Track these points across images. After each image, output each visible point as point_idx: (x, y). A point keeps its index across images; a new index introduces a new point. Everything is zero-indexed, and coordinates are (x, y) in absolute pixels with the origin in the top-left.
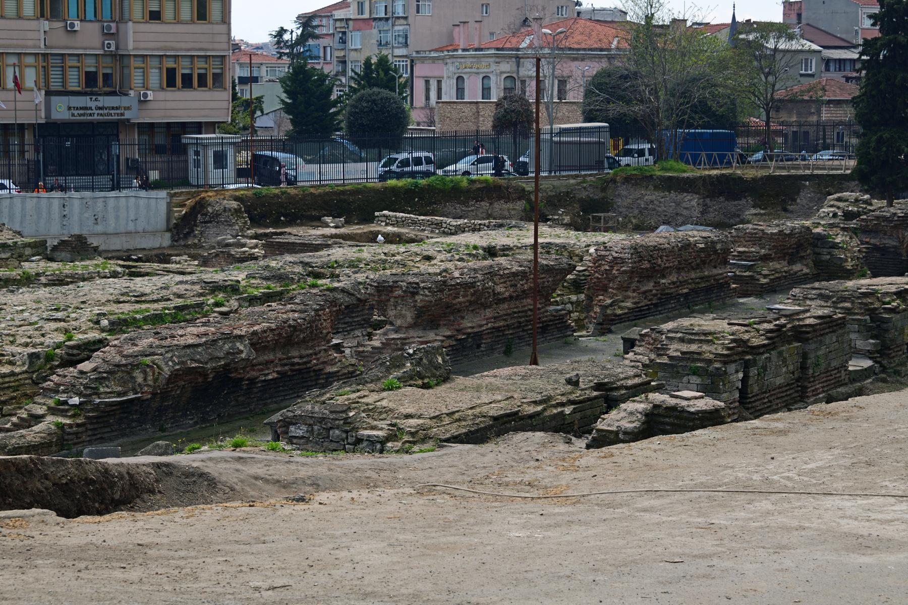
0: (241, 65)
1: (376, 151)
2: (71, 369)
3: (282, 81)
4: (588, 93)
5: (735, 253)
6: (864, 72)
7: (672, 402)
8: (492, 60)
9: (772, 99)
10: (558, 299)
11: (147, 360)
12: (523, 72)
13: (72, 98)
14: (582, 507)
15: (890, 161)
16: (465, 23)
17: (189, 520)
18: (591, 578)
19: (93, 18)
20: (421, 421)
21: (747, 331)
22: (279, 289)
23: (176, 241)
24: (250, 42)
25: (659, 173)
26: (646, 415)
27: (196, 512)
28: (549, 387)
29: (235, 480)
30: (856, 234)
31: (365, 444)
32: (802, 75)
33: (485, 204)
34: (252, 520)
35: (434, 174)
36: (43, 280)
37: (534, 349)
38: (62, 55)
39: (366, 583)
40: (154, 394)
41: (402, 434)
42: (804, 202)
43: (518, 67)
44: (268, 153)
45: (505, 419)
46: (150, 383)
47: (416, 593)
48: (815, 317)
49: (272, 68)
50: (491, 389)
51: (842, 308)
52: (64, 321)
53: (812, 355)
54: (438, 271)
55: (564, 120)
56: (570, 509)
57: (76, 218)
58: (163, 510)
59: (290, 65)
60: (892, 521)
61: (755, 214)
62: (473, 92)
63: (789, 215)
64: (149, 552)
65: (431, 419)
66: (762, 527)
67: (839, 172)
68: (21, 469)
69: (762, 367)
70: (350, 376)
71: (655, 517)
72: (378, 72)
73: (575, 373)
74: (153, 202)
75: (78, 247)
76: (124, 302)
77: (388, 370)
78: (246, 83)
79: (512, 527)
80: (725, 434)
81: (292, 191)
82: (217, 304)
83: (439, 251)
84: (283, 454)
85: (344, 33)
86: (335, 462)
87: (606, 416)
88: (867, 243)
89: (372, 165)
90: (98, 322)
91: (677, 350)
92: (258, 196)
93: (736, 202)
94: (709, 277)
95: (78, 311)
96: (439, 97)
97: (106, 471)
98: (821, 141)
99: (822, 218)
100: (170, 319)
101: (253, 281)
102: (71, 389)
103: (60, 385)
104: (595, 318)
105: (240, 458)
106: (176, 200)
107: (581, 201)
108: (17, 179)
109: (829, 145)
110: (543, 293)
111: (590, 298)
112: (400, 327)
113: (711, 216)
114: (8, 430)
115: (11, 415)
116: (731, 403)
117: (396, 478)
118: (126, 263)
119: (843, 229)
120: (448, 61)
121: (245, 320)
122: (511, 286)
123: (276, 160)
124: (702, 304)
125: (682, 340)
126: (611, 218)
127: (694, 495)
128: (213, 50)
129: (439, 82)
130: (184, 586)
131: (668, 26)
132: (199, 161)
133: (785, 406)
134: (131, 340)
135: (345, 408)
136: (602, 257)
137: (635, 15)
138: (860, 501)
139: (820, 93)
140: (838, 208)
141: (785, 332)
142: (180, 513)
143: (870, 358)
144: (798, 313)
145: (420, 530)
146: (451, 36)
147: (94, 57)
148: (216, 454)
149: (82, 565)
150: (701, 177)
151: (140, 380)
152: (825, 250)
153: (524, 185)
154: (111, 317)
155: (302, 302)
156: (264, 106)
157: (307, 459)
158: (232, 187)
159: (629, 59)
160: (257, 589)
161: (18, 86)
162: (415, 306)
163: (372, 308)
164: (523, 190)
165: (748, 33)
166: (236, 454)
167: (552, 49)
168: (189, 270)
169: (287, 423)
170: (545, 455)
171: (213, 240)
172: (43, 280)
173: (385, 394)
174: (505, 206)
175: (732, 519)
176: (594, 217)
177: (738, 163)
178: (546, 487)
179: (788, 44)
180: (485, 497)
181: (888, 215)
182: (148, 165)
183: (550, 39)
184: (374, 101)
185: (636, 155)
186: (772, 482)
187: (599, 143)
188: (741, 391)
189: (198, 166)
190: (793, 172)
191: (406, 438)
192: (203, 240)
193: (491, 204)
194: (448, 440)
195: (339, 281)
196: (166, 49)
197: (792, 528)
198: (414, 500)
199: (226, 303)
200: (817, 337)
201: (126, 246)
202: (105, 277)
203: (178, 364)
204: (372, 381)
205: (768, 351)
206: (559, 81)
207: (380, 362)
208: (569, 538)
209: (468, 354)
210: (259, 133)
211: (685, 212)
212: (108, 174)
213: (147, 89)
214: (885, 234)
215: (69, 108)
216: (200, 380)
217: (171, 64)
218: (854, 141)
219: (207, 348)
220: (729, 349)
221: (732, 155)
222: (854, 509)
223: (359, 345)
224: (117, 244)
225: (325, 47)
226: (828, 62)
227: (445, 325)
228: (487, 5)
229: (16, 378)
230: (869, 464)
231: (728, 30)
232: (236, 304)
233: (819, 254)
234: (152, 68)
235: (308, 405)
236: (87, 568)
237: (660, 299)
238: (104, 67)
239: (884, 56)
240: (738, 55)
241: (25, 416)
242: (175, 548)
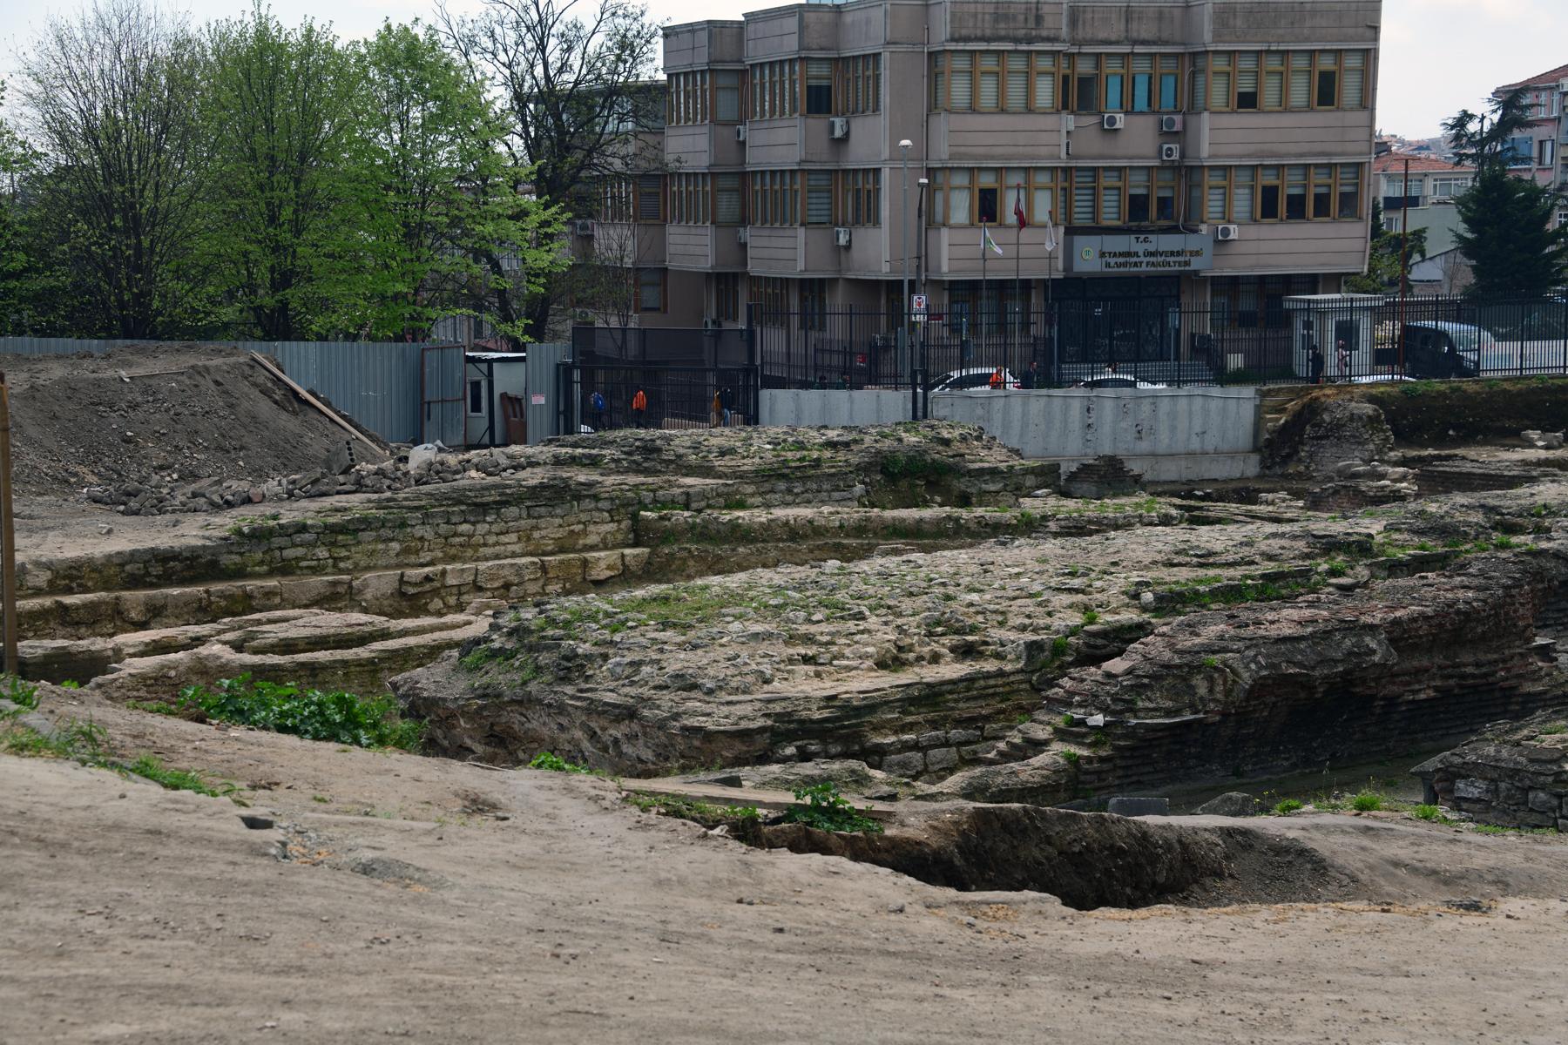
0: (1390, 178)
2: (1093, 669)
3: (1460, 202)
11: (1216, 659)
17: (1278, 927)
19: (1145, 109)
22: (1440, 550)
24: (1408, 138)
27: (1291, 914)
29: (1360, 865)
38: (1094, 169)
40: (1225, 715)
44: (1431, 324)
46: (1219, 696)
49: (1444, 180)
52: (1083, 592)
58: (1235, 907)
64: (1212, 975)
68: (1008, 824)
74: (1232, 405)
75: (1109, 475)
81: (1469, 386)
82: (1333, 573)
84: (1444, 827)
92: (1409, 394)
100: (1254, 594)
101: (1396, 536)
102: (1092, 701)
105: (1368, 829)
114: (991, 762)
115: (997, 738)
121: (1381, 599)
123: (1444, 335)
128: (1342, 154)
132: (1310, 337)
135: (1557, 755)
142: (1262, 914)
148: (1327, 819)
149: (1101, 988)
151: (1202, 690)
154: (1159, 589)
156: (1427, 245)
157: (1486, 839)
158: (1365, 380)
166: (1362, 822)
168: (1289, 515)
169: (1451, 775)
171: (1331, 467)
172: (1053, 526)
192: (1313, 466)
195: (1549, 539)
202: (1151, 524)
203: (1265, 668)
210: (1416, 291)
213: (1230, 222)
215: (1102, 255)
216: (1302, 695)
217: (1269, 180)
224: (1170, 471)
225: (1541, 143)
232: (1366, 573)
235: (1490, 746)
236: (1108, 994)
241: (1017, 741)
242: (1254, 971)
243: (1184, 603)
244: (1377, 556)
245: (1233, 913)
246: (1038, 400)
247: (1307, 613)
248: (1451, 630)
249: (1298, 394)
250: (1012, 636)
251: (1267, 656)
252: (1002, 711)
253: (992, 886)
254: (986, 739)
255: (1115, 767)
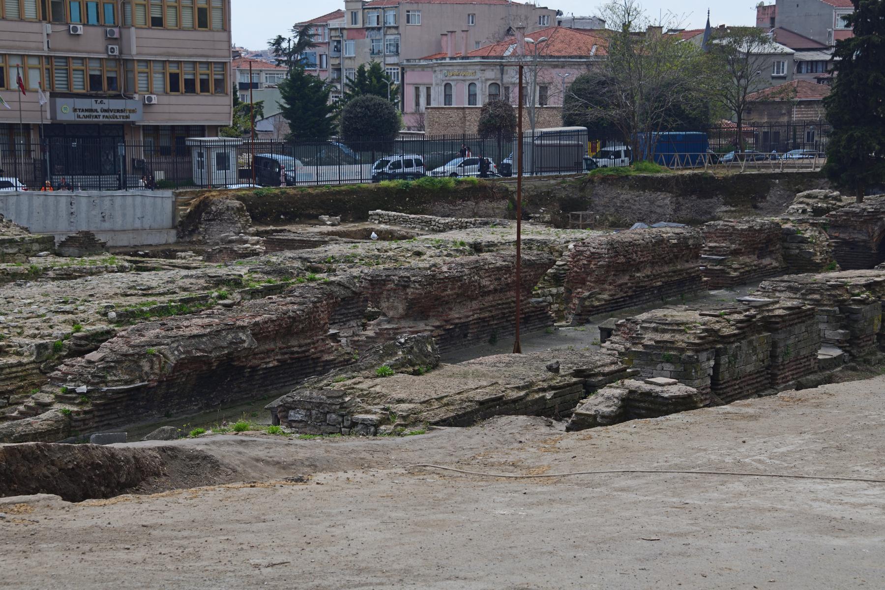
0: (242, 72)
1: (370, 153)
2: (79, 359)
3: (281, 87)
4: (568, 99)
5: (707, 248)
6: (836, 73)
7: (647, 387)
8: (478, 67)
9: (744, 101)
10: (539, 292)
11: (154, 350)
12: (507, 79)
13: (77, 100)
14: (562, 486)
15: (861, 158)
16: (452, 32)
17: (192, 501)
18: (572, 554)
19: (95, 23)
20: (412, 406)
21: (718, 322)
22: (279, 283)
23: (182, 238)
24: (250, 49)
25: (634, 174)
26: (623, 400)
27: (200, 493)
28: (531, 374)
29: (238, 462)
30: (825, 229)
31: (360, 427)
32: (773, 78)
33: (471, 204)
34: (253, 500)
35: (424, 175)
36: (51, 274)
37: (517, 338)
38: (66, 58)
39: (360, 559)
40: (160, 382)
41: (395, 417)
42: (774, 199)
43: (502, 74)
44: (269, 155)
45: (490, 404)
46: (157, 371)
47: (407, 568)
48: (784, 308)
49: (271, 75)
50: (478, 375)
51: (811, 300)
52: (72, 313)
53: (781, 345)
54: (428, 266)
55: (546, 124)
56: (551, 488)
57: (83, 215)
58: (167, 492)
59: (288, 72)
60: (865, 505)
61: (726, 212)
62: (460, 99)
63: (758, 212)
64: (154, 533)
65: (421, 403)
66: (735, 508)
67: (809, 170)
68: (27, 456)
69: (733, 355)
70: (346, 364)
71: (631, 497)
72: (371, 79)
73: (555, 360)
74: (159, 201)
75: (86, 243)
76: (131, 295)
77: (381, 358)
78: (246, 89)
79: (497, 504)
80: (698, 418)
81: (291, 191)
82: (221, 297)
83: (429, 247)
84: (283, 437)
85: (339, 42)
86: (331, 444)
87: (584, 401)
88: (836, 237)
89: (366, 167)
90: (105, 314)
91: (651, 339)
92: (258, 195)
93: (707, 200)
94: (682, 270)
95: (86, 304)
96: (428, 103)
97: (113, 455)
98: (791, 141)
99: (792, 215)
100: (175, 311)
101: (255, 275)
102: (79, 378)
103: (68, 374)
104: (574, 310)
105: (243, 441)
106: (181, 199)
107: (561, 200)
108: (24, 177)
109: (799, 144)
110: (525, 287)
111: (569, 291)
112: (392, 318)
113: (683, 213)
114: (15, 418)
115: (18, 404)
116: (703, 389)
117: (389, 459)
118: (133, 258)
119: (813, 225)
120: (437, 69)
121: (248, 311)
122: (496, 279)
123: (275, 162)
124: (675, 296)
125: (655, 330)
126: (590, 216)
127: (669, 475)
128: (214, 57)
129: (428, 89)
130: (187, 565)
131: (644, 33)
132: (202, 162)
133: (756, 392)
134: (138, 330)
135: (341, 393)
136: (581, 253)
137: (613, 24)
138: (832, 485)
139: (791, 95)
140: (808, 204)
141: (755, 322)
142: (184, 494)
143: (840, 348)
144: (767, 304)
145: (411, 508)
146: (439, 44)
147: (98, 61)
148: (219, 438)
149: (86, 547)
150: (674, 177)
151: (147, 368)
152: (794, 245)
153: (508, 186)
154: (119, 310)
155: (301, 295)
156: (264, 111)
157: (305, 442)
158: (234, 187)
159: (607, 66)
160: (257, 566)
161: (23, 87)
162: (406, 299)
163: (366, 300)
164: (507, 190)
165: (722, 38)
166: (238, 438)
167: (534, 57)
168: (194, 265)
169: (287, 408)
170: (528, 437)
171: (217, 237)
172: (51, 274)
173: (378, 380)
174: (490, 205)
175: (706, 499)
176: (572, 215)
177: (710, 163)
178: (529, 468)
179: (761, 48)
180: (471, 476)
181: (858, 210)
182: (154, 166)
183: (532, 47)
184: (367, 107)
185: (612, 157)
186: (744, 465)
187: (578, 145)
188: (712, 378)
189: (202, 167)
190: (763, 171)
191: (398, 421)
192: (207, 237)
193: (477, 203)
194: (437, 423)
195: (335, 275)
196: (169, 55)
197: (765, 509)
198: (405, 479)
199: (230, 296)
200: (786, 327)
201: (133, 242)
202: (113, 272)
203: (183, 353)
204: (366, 369)
205: (738, 340)
206: (541, 87)
207: (374, 350)
208: (550, 516)
209: (456, 343)
210: (259, 137)
211: (659, 210)
212: (115, 174)
213: (151, 93)
214: (855, 229)
215: (75, 110)
216: (205, 368)
217: (174, 70)
218: (825, 140)
219: (211, 338)
220: (700, 338)
221: (704, 156)
222: (826, 492)
223: (354, 334)
224: (124, 240)
225: (321, 55)
226: (800, 64)
227: (434, 316)
228: (473, 15)
229: (23, 368)
230: (840, 449)
231: (702, 36)
232: (239, 297)
233: (788, 248)
234: (155, 73)
235: (307, 391)
236: (91, 550)
237: (635, 291)
238: (108, 71)
239: (857, 56)
240: (712, 60)
241: (32, 404)
242: (179, 528)
243: (135, 318)
244: (245, 287)
245: (167, 496)
246: (38, 198)
247: (207, 321)
248: (286, 328)
249: (197, 194)
250: (27, 341)
251: (184, 347)
252: (22, 387)
253: (16, 493)
254: (11, 404)
255: (94, 417)
